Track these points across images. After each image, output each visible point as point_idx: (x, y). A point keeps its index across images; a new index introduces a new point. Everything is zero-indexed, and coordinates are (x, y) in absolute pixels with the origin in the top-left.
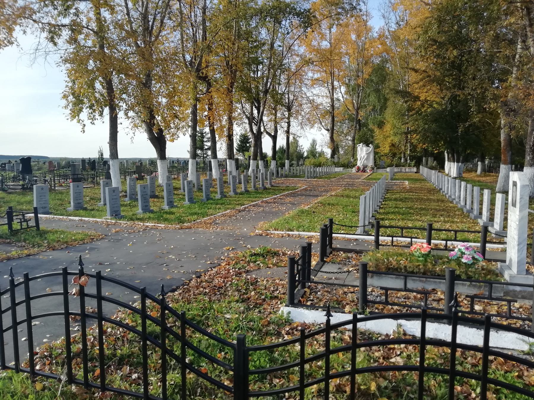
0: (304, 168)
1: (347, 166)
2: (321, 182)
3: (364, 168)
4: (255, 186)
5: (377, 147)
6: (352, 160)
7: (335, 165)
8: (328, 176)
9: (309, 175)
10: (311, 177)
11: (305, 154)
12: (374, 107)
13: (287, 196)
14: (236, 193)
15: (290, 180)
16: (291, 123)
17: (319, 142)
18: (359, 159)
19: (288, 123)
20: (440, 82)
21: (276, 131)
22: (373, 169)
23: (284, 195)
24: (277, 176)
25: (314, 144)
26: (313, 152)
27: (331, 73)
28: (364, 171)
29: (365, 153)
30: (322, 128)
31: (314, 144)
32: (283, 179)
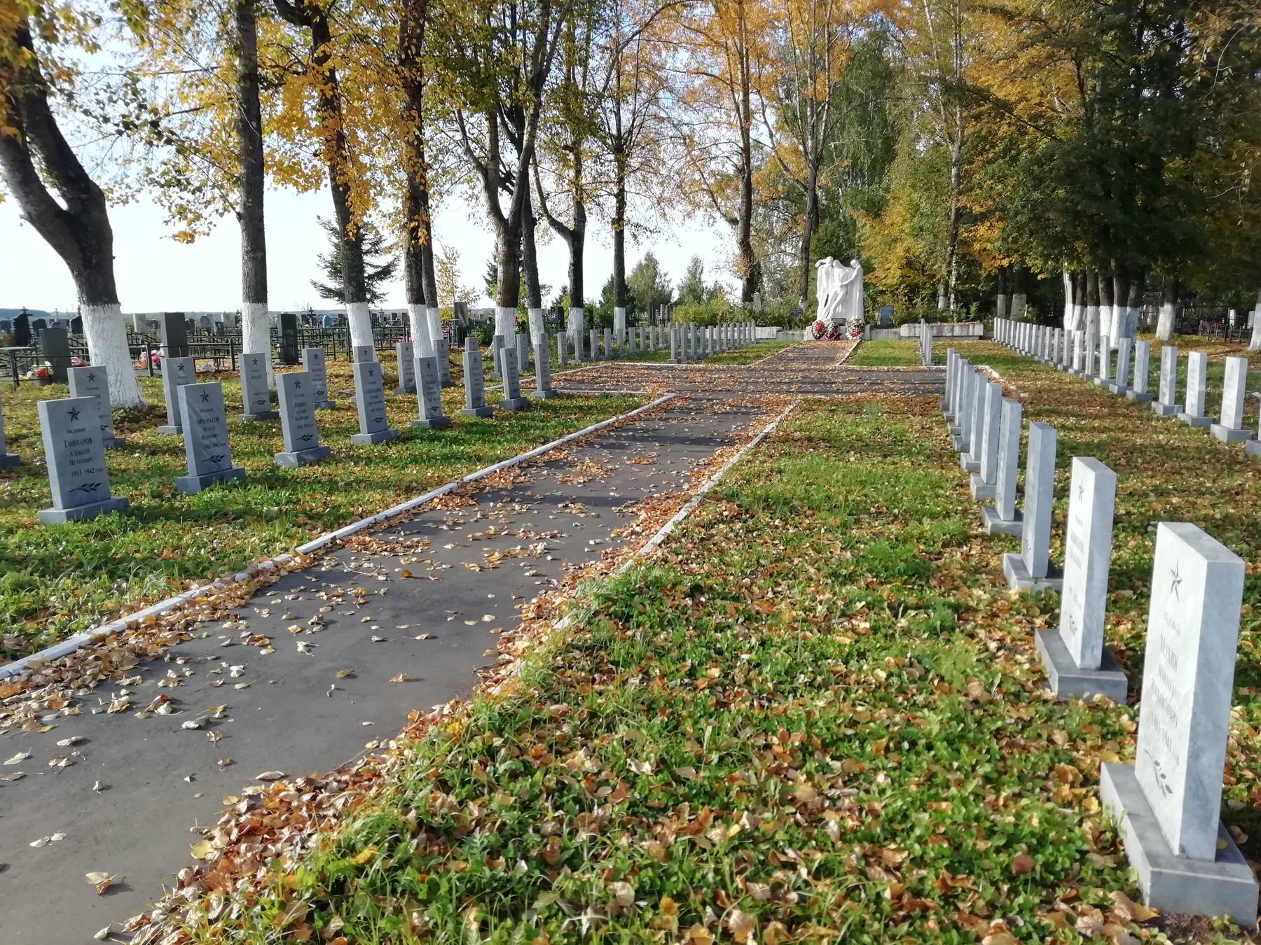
0: (667, 330)
1: (789, 322)
2: (720, 374)
3: (836, 327)
4: (477, 400)
5: (867, 268)
6: (802, 306)
7: (755, 318)
8: (737, 353)
9: (682, 350)
10: (689, 359)
11: (675, 296)
12: (855, 159)
13: (586, 444)
14: (383, 434)
15: (620, 369)
16: (629, 198)
17: (707, 266)
18: (821, 301)
19: (616, 196)
20: (1081, 48)
21: (581, 218)
22: (861, 328)
23: (576, 441)
24: (586, 357)
25: (696, 269)
26: (693, 290)
27: (740, 53)
28: (836, 335)
29: (837, 284)
30: (718, 215)
31: (696, 269)
32: (602, 364)
